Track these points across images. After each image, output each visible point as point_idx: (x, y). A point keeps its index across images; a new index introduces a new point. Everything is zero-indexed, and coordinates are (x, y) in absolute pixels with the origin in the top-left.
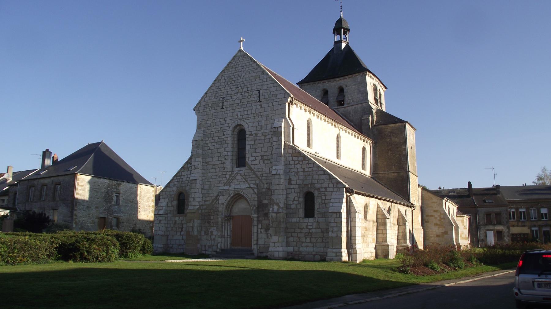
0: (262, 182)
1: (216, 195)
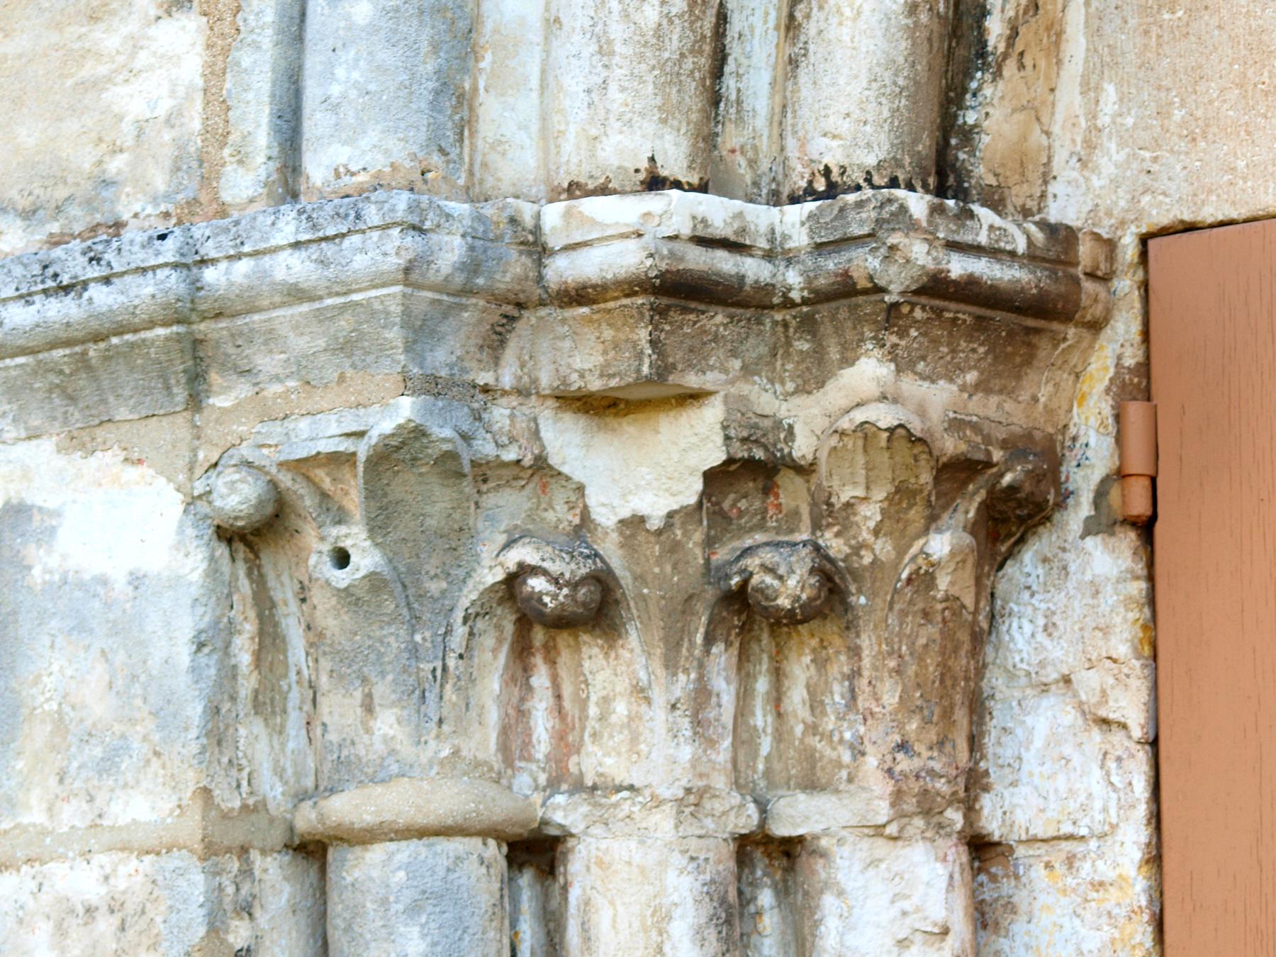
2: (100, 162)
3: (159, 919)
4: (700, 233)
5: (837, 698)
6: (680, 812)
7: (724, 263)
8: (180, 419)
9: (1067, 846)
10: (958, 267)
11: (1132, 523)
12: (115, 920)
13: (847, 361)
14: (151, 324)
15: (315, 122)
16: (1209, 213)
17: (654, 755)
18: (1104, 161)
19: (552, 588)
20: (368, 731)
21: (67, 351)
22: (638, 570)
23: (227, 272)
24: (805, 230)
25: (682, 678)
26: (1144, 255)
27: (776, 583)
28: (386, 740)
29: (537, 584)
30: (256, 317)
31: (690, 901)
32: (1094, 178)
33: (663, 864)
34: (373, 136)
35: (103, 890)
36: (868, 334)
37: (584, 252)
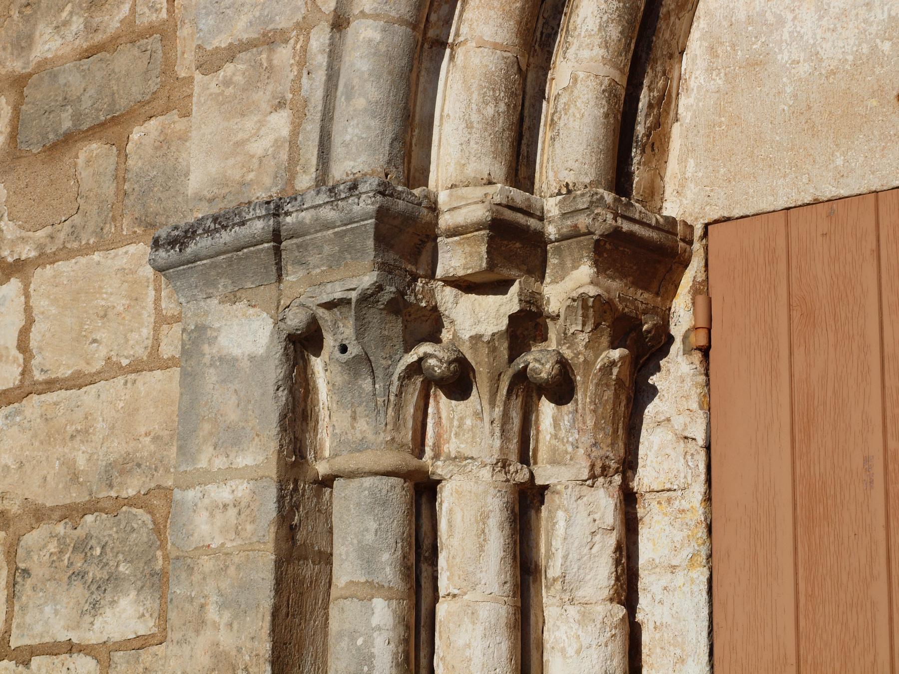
2: (243, 176)
3: (256, 509)
4: (510, 204)
5: (566, 423)
6: (494, 470)
7: (521, 218)
8: (273, 287)
9: (666, 494)
10: (626, 226)
11: (699, 349)
12: (236, 510)
13: (575, 268)
14: (262, 242)
15: (338, 150)
16: (736, 213)
17: (483, 444)
18: (688, 192)
19: (439, 364)
20: (353, 428)
21: (224, 257)
22: (478, 360)
23: (297, 217)
24: (557, 208)
25: (497, 409)
26: (705, 234)
27: (540, 367)
28: (362, 432)
29: (432, 362)
30: (308, 237)
31: (498, 510)
32: (684, 200)
33: (486, 492)
34: (363, 158)
35: (231, 497)
36: (585, 254)
37: (457, 211)
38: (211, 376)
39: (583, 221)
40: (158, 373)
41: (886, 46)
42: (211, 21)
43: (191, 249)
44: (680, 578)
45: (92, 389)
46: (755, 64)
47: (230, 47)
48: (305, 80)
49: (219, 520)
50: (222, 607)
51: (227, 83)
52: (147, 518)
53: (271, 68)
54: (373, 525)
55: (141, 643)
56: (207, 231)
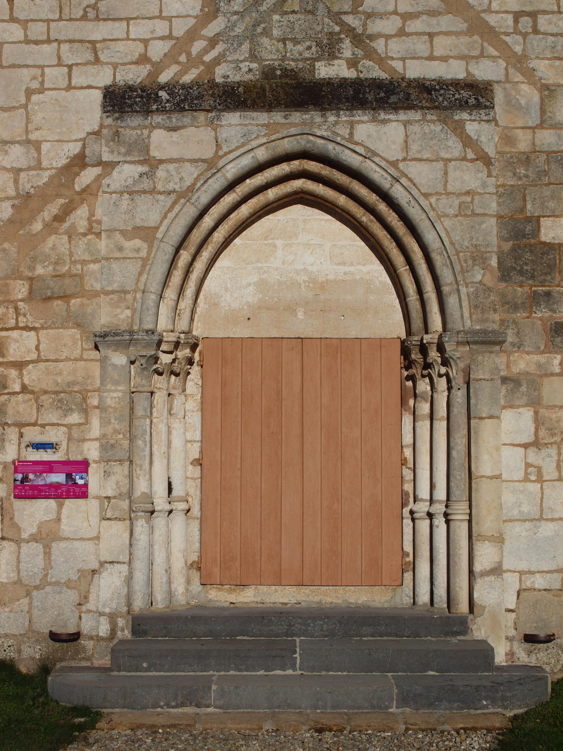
0: (530, 75)
1: (57, 156)
16: (210, 337)
38: (110, 368)
39: (190, 341)
40: (83, 362)
41: (246, 307)
42: (106, 283)
43: (107, 339)
44: (195, 414)
45: (62, 363)
46: (216, 304)
47: (112, 291)
48: (135, 304)
49: (114, 400)
50: (115, 420)
51: (112, 299)
52: (81, 396)
53: (125, 299)
54: (146, 403)
55: (80, 424)
56: (112, 336)
